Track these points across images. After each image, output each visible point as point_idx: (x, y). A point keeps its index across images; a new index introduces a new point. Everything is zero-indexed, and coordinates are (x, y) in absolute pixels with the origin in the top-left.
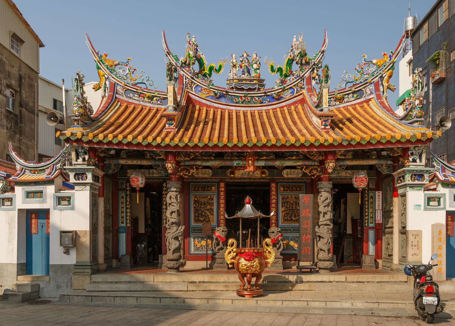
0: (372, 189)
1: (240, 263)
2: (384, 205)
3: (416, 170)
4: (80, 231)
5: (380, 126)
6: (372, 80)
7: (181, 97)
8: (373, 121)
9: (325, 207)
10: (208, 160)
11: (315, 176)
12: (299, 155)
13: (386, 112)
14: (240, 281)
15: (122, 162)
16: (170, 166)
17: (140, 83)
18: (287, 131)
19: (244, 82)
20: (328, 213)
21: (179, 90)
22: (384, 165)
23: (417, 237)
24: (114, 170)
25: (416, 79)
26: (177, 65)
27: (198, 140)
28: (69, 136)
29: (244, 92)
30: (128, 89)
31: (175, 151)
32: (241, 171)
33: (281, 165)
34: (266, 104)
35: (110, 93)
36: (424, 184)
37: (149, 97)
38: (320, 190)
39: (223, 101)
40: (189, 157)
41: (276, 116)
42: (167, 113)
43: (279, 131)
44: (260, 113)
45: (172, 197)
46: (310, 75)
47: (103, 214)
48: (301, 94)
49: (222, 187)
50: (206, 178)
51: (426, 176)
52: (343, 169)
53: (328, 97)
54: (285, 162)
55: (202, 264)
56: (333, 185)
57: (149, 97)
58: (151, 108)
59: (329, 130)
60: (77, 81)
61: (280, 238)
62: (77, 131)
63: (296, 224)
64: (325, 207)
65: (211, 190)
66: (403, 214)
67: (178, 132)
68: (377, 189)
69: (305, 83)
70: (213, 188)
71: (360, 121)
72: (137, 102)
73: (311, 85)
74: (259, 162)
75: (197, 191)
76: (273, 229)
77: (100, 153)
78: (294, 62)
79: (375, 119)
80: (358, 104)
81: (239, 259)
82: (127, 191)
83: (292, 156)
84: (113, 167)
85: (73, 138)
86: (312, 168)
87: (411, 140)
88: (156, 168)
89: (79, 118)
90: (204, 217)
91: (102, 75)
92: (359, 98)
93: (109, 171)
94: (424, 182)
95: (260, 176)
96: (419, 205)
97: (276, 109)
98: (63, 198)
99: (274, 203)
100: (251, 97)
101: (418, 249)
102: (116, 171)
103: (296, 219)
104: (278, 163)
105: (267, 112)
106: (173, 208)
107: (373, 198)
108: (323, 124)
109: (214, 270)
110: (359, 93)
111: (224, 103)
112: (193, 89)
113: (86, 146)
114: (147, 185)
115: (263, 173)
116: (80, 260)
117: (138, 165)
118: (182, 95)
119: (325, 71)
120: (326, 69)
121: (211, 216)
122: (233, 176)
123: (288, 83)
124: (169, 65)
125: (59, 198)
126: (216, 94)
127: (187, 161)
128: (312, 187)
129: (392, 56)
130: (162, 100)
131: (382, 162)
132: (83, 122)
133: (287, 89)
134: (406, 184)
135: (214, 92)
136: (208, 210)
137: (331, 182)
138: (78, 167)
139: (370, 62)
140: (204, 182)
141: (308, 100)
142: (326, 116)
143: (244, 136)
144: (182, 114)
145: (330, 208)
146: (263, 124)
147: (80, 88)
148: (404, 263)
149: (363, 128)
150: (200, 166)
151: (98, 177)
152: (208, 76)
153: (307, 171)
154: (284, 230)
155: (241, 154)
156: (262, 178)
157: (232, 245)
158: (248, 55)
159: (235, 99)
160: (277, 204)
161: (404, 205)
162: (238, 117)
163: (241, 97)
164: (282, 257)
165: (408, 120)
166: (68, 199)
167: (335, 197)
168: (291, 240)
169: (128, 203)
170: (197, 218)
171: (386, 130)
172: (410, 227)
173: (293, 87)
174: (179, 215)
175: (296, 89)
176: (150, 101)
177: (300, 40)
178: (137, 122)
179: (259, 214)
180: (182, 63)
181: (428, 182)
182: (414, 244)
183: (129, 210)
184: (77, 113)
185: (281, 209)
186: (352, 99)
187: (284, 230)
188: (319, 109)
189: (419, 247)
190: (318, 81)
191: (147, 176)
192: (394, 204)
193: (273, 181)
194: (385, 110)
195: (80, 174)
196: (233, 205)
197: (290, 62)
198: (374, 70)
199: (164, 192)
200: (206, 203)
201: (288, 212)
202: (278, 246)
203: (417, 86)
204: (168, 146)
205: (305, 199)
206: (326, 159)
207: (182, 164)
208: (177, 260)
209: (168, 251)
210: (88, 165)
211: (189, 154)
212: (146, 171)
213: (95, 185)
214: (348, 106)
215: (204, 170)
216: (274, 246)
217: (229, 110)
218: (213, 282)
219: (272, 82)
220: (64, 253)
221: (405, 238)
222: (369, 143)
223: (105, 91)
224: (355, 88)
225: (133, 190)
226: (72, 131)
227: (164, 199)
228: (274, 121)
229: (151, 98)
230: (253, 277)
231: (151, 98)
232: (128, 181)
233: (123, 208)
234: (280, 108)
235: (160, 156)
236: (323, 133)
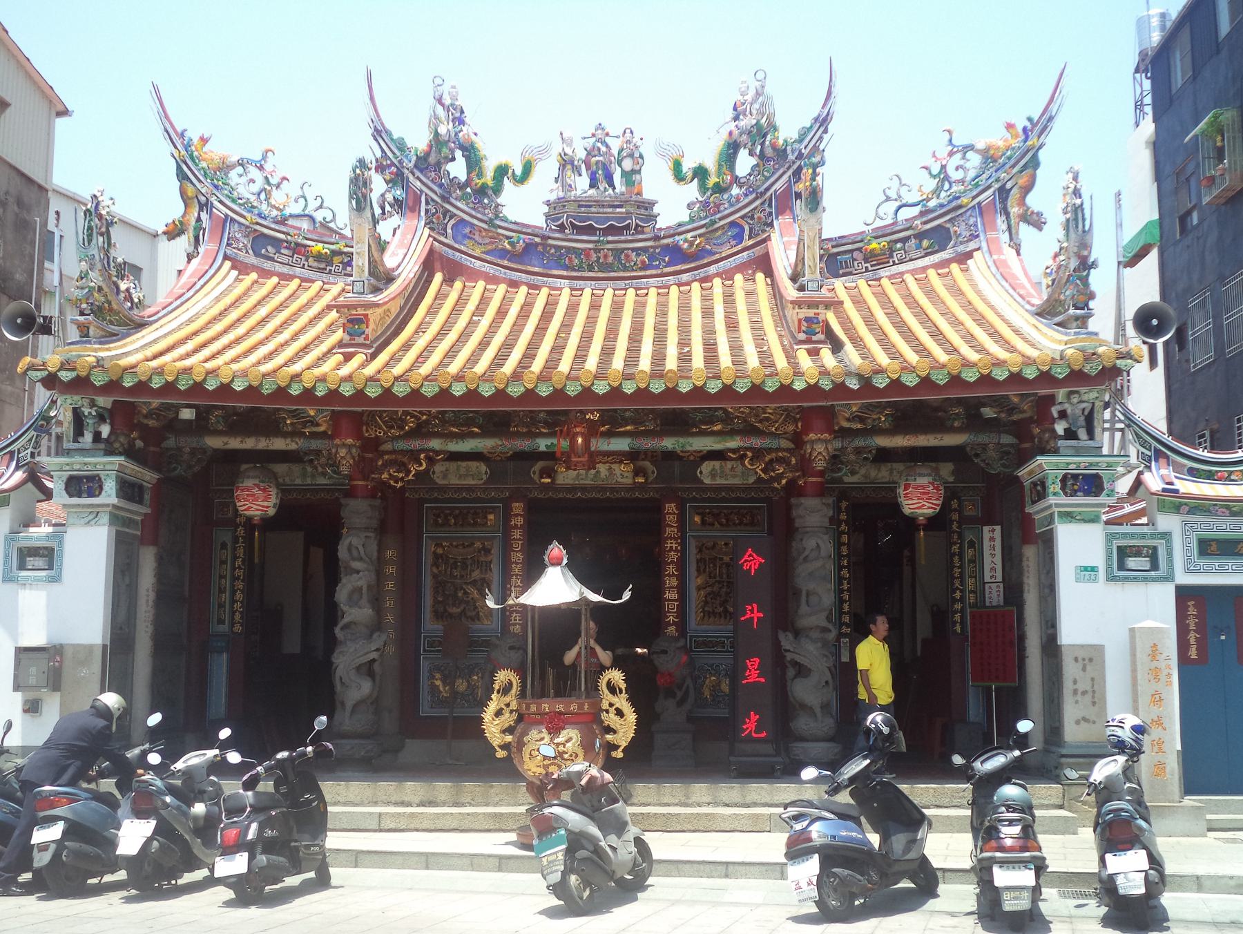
6: (974, 198)
10: (462, 436)
15: (215, 442)
17: (298, 216)
23: (1089, 668)
28: (54, 370)
30: (263, 235)
31: (360, 409)
37: (319, 257)
40: (402, 428)
47: (152, 596)
50: (469, 489)
52: (865, 459)
54: (690, 440)
70: (491, 517)
71: (508, 346)
74: (613, 440)
75: (442, 525)
77: (146, 417)
78: (743, 154)
82: (237, 526)
83: (712, 423)
86: (773, 455)
88: (311, 461)
93: (175, 469)
95: (629, 481)
96: (1093, 569)
99: (672, 562)
100: (617, 250)
101: (1094, 703)
104: (668, 443)
107: (976, 545)
108: (804, 328)
111: (536, 269)
112: (449, 231)
113: (104, 401)
114: (282, 507)
115: (637, 472)
117: (261, 451)
129: (1032, 131)
131: (983, 438)
136: (474, 583)
150: (437, 453)
151: (141, 487)
152: (490, 192)
154: (705, 644)
156: (636, 487)
159: (570, 259)
169: (239, 562)
170: (441, 609)
175: (747, 228)
176: (322, 266)
182: (1081, 687)
183: (240, 585)
184: (84, 306)
187: (705, 644)
189: (1096, 696)
197: (732, 148)
200: (469, 562)
207: (387, 447)
219: (673, 205)
223: (197, 239)
224: (925, 223)
233: (225, 577)
234: (937, 266)
235: (318, 425)
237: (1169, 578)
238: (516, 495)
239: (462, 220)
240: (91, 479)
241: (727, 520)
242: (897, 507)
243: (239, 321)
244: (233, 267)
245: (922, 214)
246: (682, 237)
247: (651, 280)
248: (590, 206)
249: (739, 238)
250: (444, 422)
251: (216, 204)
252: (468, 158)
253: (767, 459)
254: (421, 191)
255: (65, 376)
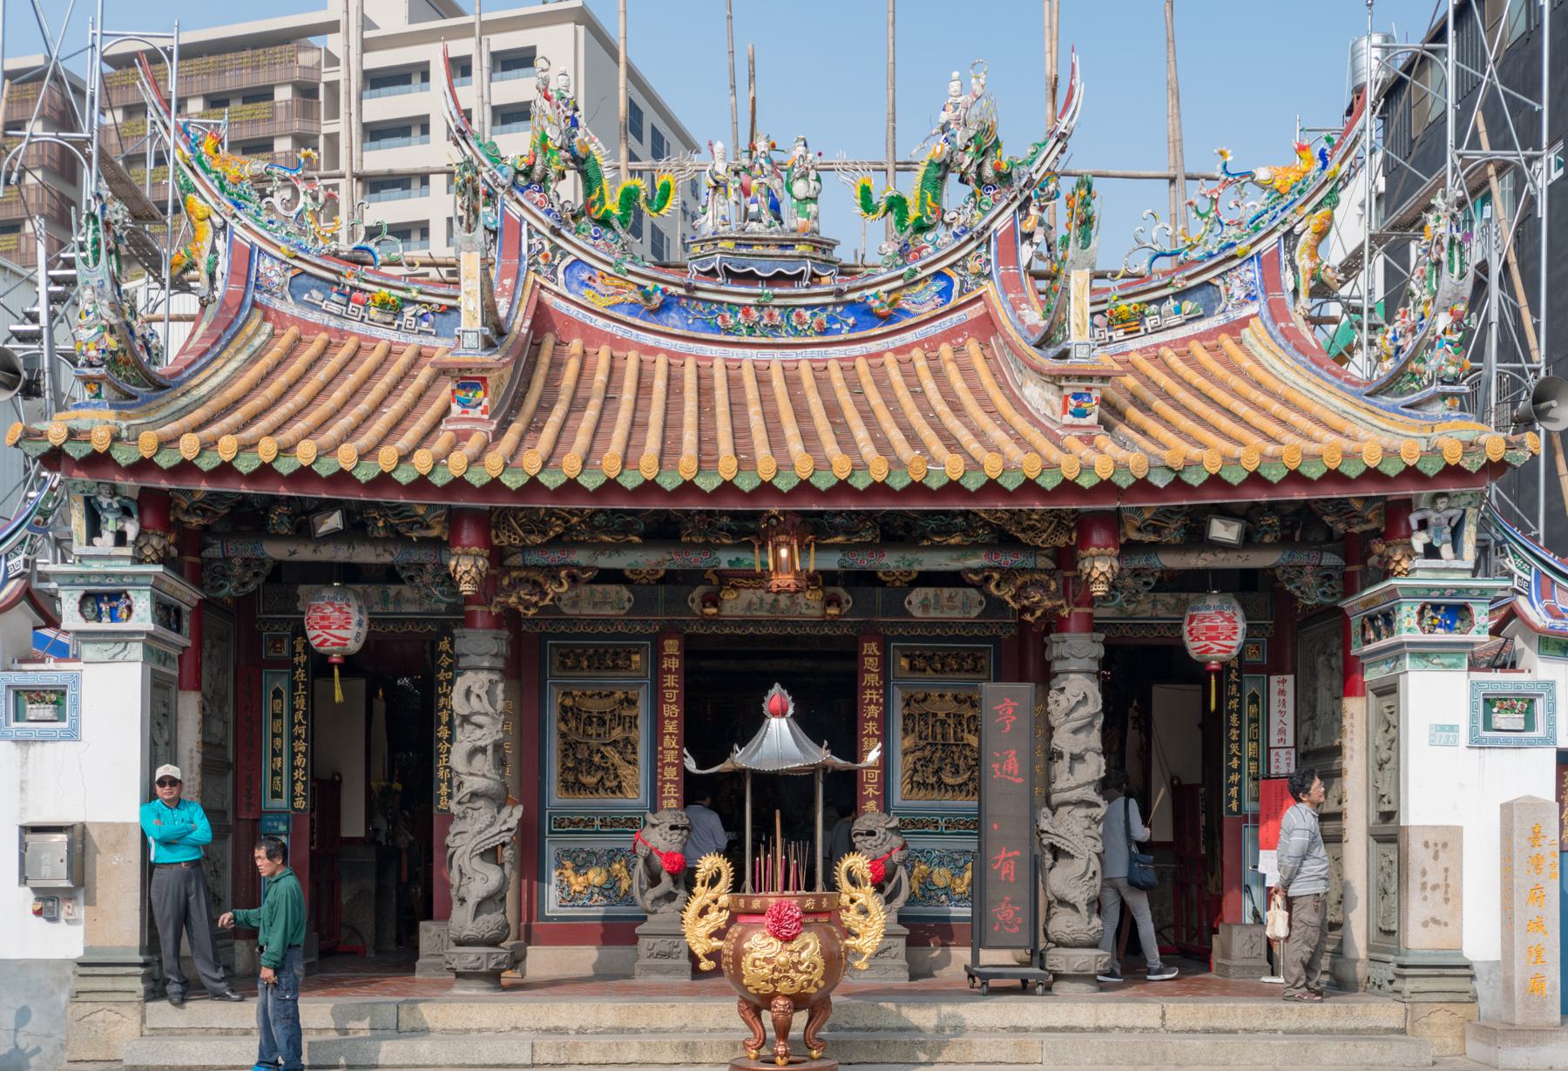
0: (1255, 669)
1: (743, 952)
2: (1305, 729)
3: (1438, 588)
4: (100, 824)
5: (1293, 417)
6: (1253, 245)
7: (512, 304)
8: (1262, 399)
9: (1076, 731)
10: (617, 548)
11: (1038, 613)
12: (975, 530)
13: (1308, 368)
14: (741, 1024)
15: (276, 551)
16: (467, 567)
18: (927, 434)
19: (757, 249)
20: (1089, 756)
21: (502, 276)
22: (1308, 569)
24: (244, 585)
25: (1441, 230)
26: (495, 181)
27: (578, 465)
29: (759, 291)
30: (304, 272)
32: (747, 595)
33: (903, 568)
34: (841, 338)
35: (233, 287)
36: (1472, 644)
37: (383, 305)
38: (1057, 666)
39: (673, 322)
40: (545, 533)
41: (883, 384)
42: (455, 359)
43: (896, 436)
44: (821, 374)
45: (475, 689)
46: (1014, 224)
48: (979, 298)
49: (670, 656)
50: (607, 621)
51: (1482, 616)
52: (1146, 584)
53: (1089, 310)
54: (920, 556)
55: (584, 957)
56: (1107, 645)
57: (383, 305)
58: (394, 348)
59: (1095, 432)
60: (95, 221)
61: (896, 857)
62: (97, 423)
63: (958, 803)
64: (1076, 731)
65: (628, 668)
66: (1387, 762)
67: (499, 433)
68: (1276, 666)
69: (992, 257)
70: (636, 658)
72: (334, 323)
73: (1016, 262)
75: (572, 668)
76: (870, 816)
77: (187, 512)
78: (953, 178)
79: (1272, 394)
80: (1199, 337)
81: (741, 938)
82: (295, 668)
83: (950, 533)
84: (237, 570)
85: (76, 451)
86: (1027, 578)
87: (1420, 467)
88: (411, 578)
89: (103, 371)
90: (599, 774)
91: (201, 215)
92: (1200, 317)
93: (222, 586)
94: (1472, 636)
96: (1453, 728)
97: (879, 355)
98: (36, 694)
99: (872, 719)
100: (786, 307)
101: (1447, 900)
102: (251, 587)
103: (960, 780)
105: (848, 367)
106: (479, 733)
107: (1261, 700)
108: (1071, 408)
109: (639, 981)
110: (1203, 293)
112: (561, 276)
113: (130, 485)
114: (373, 644)
115: (830, 601)
116: (99, 942)
118: (514, 296)
119: (1078, 200)
120: (1083, 192)
121: (626, 770)
122: (714, 610)
123: (929, 254)
124: (466, 169)
125: (17, 693)
126: (647, 297)
127: (537, 547)
128: (1024, 656)
130: (439, 317)
131: (1301, 558)
132: (117, 388)
133: (924, 279)
134: (1401, 645)
135: (640, 287)
136: (614, 743)
137: (1102, 636)
138: (97, 567)
139: (1243, 175)
140: (601, 636)
141: (1005, 321)
142: (1080, 378)
143: (762, 451)
144: (516, 370)
145: (1094, 739)
146: (833, 411)
147: (110, 252)
148: (1391, 958)
149: (1225, 423)
150: (584, 569)
151: (178, 611)
152: (615, 223)
153: (1006, 594)
155: (744, 518)
156: (825, 621)
157: (714, 882)
158: (773, 146)
159: (723, 318)
160: (884, 722)
161: (1390, 726)
162: (734, 383)
163: (746, 308)
164: (907, 932)
165: (1402, 394)
166: (54, 697)
167: (1186, 661)
168: (941, 864)
169: (299, 716)
170: (571, 779)
171: (1318, 432)
172: (1417, 812)
173: (948, 272)
174: (501, 763)
175: (956, 280)
176: (389, 319)
177: (976, 87)
178: (338, 394)
179: (821, 755)
180: (518, 172)
181: (1485, 637)
182: (1431, 879)
183: (301, 746)
184: (93, 353)
185: (900, 742)
186: (1176, 320)
188: (1052, 351)
189: (1450, 891)
190: (1043, 249)
191: (377, 609)
192: (1346, 722)
193: (871, 632)
194: (1307, 360)
195: (103, 598)
196: (719, 719)
198: (1260, 208)
199: (442, 675)
200: (608, 717)
201: (927, 753)
202: (889, 888)
203: (1444, 256)
204: (459, 484)
205: (1004, 703)
206: (1084, 542)
207: (516, 560)
208: (494, 942)
209: (456, 904)
210: (138, 560)
211: (543, 521)
212: (374, 591)
213: (164, 641)
214: (1157, 346)
215: (600, 588)
216: (879, 887)
217: (698, 358)
218: (637, 1031)
220: (38, 913)
221: (1394, 857)
222: (1255, 479)
225: (320, 665)
226: (74, 424)
227: (442, 700)
228: (875, 399)
229: (393, 309)
230: (797, 1009)
231: (393, 309)
232: (300, 631)
233: (280, 735)
234: (898, 351)
235: (428, 527)
236: (1071, 440)
237: (1549, 740)
238: (670, 630)
239: (578, 260)
240: (115, 596)
241: (943, 665)
242: (1183, 648)
243: (291, 387)
244: (265, 319)
245: (1182, 266)
246: (873, 291)
247: (831, 350)
248: (751, 246)
249: (946, 293)
250: (593, 528)
251: (238, 229)
252: (583, 173)
253: (1019, 582)
254: (522, 218)
255: (76, 451)
